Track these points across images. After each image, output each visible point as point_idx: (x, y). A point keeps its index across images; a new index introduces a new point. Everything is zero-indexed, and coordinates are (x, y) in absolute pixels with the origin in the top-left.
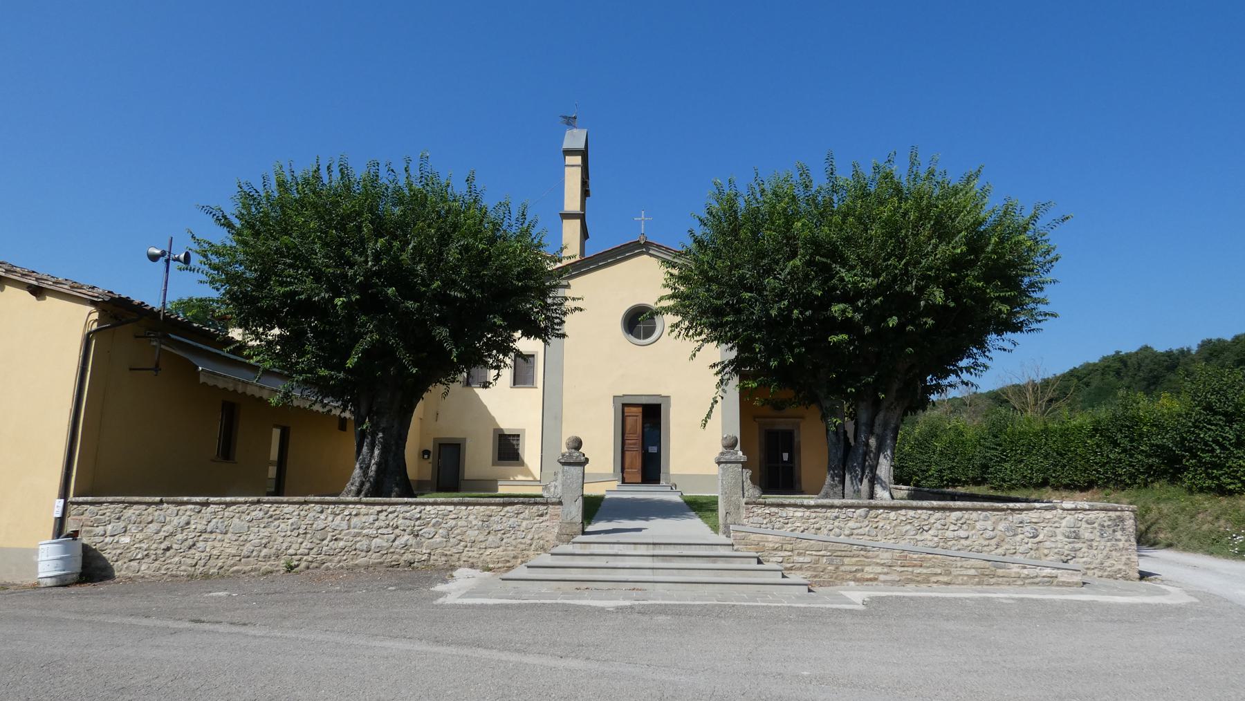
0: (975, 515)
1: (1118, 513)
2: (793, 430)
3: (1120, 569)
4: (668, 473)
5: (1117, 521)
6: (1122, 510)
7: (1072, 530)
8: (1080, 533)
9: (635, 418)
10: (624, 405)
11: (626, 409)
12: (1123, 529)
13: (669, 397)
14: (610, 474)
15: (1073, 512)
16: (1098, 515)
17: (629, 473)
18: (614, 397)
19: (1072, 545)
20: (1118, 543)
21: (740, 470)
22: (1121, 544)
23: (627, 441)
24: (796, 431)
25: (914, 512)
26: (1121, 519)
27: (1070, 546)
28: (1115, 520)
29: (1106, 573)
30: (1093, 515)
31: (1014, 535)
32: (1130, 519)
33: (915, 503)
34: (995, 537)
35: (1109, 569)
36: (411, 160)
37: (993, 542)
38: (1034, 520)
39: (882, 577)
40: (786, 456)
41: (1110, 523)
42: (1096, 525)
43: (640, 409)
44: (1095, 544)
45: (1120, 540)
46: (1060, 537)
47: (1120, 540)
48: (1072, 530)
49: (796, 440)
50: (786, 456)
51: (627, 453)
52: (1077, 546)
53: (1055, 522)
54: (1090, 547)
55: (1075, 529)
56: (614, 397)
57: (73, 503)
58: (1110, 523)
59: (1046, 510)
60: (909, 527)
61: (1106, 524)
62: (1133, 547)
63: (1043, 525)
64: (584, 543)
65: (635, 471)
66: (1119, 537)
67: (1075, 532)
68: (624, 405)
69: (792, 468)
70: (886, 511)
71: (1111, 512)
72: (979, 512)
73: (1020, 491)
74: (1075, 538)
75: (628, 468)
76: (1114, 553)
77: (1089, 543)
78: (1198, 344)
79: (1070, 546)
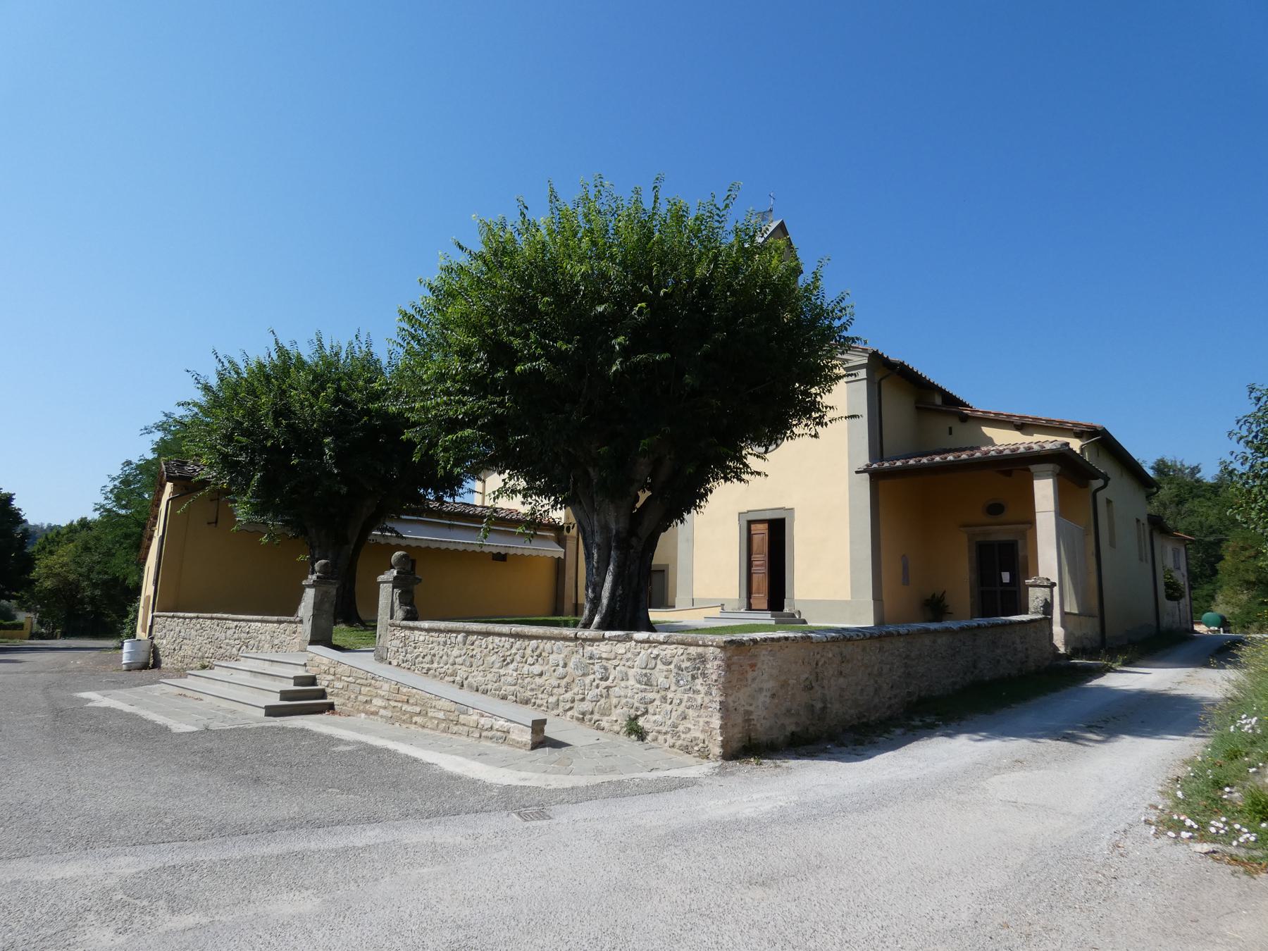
0: (548, 645)
1: (700, 650)
2: (1016, 541)
3: (696, 739)
4: (792, 598)
5: (697, 661)
6: (705, 645)
7: (644, 671)
8: (653, 677)
9: (762, 536)
10: (750, 523)
11: (753, 526)
12: (704, 675)
13: (792, 509)
14: (736, 599)
15: (647, 645)
16: (675, 651)
17: (755, 598)
18: (739, 514)
19: (644, 694)
20: (696, 696)
21: (391, 590)
22: (699, 698)
23: (755, 563)
24: (1020, 543)
25: (500, 638)
26: (702, 659)
27: (641, 695)
28: (695, 659)
29: (680, 742)
30: (669, 650)
31: (584, 675)
32: (715, 658)
33: (411, 624)
34: (565, 677)
35: (683, 736)
36: (853, 319)
37: (563, 682)
38: (604, 655)
39: (382, 712)
40: (1006, 577)
41: (688, 664)
42: (672, 666)
43: (766, 526)
44: (670, 695)
45: (698, 692)
46: (632, 682)
47: (698, 692)
48: (644, 671)
49: (1021, 554)
50: (1006, 577)
51: (754, 576)
52: (650, 696)
53: (628, 660)
54: (664, 699)
55: (648, 671)
56: (739, 514)
57: (157, 616)
58: (688, 664)
59: (619, 641)
60: (494, 657)
61: (683, 666)
62: (714, 705)
63: (615, 662)
64: (265, 660)
65: (761, 599)
66: (699, 687)
67: (645, 675)
68: (750, 523)
69: (1015, 592)
70: (479, 637)
71: (692, 648)
72: (553, 642)
73: (915, 629)
74: (646, 684)
75: (755, 593)
76: (691, 713)
77: (663, 693)
78: (86, 518)
79: (641, 695)
